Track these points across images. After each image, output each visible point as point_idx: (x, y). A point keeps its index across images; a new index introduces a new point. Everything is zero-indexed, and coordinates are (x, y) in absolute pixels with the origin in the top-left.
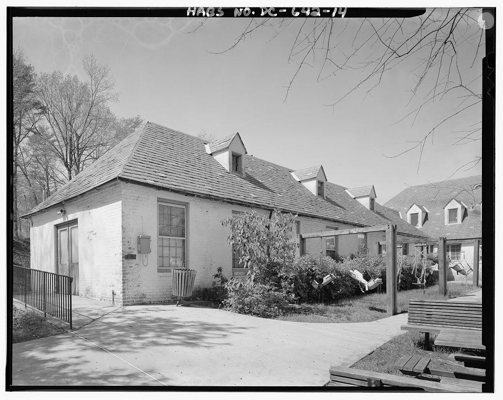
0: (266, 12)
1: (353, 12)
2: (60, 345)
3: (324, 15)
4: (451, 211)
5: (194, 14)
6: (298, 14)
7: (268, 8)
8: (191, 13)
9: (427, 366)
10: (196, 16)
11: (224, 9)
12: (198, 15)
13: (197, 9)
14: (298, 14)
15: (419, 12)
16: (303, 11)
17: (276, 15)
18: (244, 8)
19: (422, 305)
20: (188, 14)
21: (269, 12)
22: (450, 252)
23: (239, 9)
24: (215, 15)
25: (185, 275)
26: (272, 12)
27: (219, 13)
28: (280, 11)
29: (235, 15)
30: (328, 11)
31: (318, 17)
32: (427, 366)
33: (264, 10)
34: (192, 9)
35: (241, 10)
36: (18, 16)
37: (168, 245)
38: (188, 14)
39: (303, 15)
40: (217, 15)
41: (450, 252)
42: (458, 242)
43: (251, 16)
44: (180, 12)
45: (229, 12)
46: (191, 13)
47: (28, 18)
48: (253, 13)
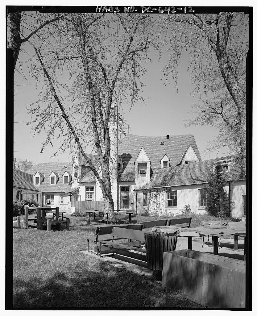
0: (145, 11)
2: (32, 214)
4: (164, 162)
7: (147, 7)
9: (190, 224)
11: (120, 7)
12: (103, 12)
13: (103, 7)
17: (152, 12)
18: (130, 7)
20: (96, 11)
21: (147, 10)
22: (50, 199)
23: (127, 7)
24: (114, 12)
27: (116, 10)
28: (178, 9)
32: (190, 224)
33: (144, 9)
34: (99, 7)
35: (129, 8)
36: (85, 6)
40: (115, 12)
41: (50, 199)
42: (52, 194)
43: (134, 12)
44: (91, 9)
48: (136, 10)
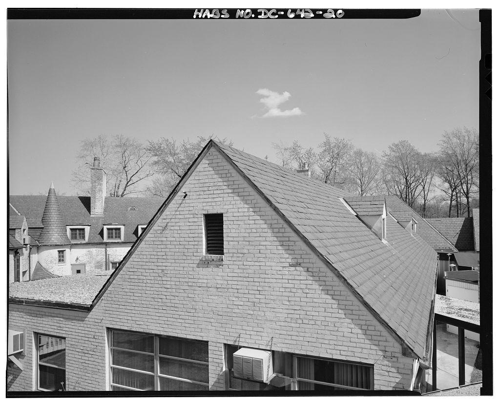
1: (350, 14)
3: (317, 16)
5: (200, 17)
6: (292, 16)
7: (269, 10)
8: (197, 16)
10: (202, 18)
14: (292, 16)
15: (415, 13)
16: (298, 12)
17: (277, 16)
18: (245, 10)
19: (295, 258)
25: (210, 226)
26: (273, 14)
29: (237, 17)
30: (321, 13)
31: (332, 18)
37: (396, 289)
38: (195, 17)
39: (298, 17)
44: (186, 14)
45: (232, 13)
46: (197, 16)
47: (358, 8)
